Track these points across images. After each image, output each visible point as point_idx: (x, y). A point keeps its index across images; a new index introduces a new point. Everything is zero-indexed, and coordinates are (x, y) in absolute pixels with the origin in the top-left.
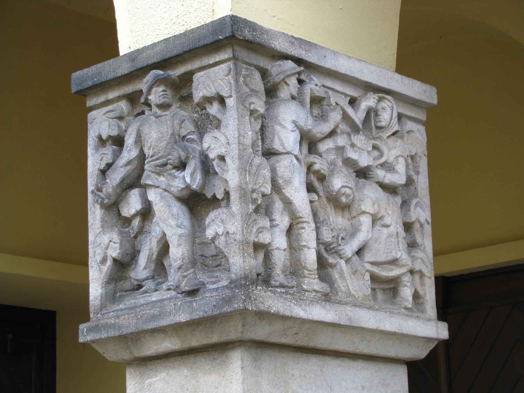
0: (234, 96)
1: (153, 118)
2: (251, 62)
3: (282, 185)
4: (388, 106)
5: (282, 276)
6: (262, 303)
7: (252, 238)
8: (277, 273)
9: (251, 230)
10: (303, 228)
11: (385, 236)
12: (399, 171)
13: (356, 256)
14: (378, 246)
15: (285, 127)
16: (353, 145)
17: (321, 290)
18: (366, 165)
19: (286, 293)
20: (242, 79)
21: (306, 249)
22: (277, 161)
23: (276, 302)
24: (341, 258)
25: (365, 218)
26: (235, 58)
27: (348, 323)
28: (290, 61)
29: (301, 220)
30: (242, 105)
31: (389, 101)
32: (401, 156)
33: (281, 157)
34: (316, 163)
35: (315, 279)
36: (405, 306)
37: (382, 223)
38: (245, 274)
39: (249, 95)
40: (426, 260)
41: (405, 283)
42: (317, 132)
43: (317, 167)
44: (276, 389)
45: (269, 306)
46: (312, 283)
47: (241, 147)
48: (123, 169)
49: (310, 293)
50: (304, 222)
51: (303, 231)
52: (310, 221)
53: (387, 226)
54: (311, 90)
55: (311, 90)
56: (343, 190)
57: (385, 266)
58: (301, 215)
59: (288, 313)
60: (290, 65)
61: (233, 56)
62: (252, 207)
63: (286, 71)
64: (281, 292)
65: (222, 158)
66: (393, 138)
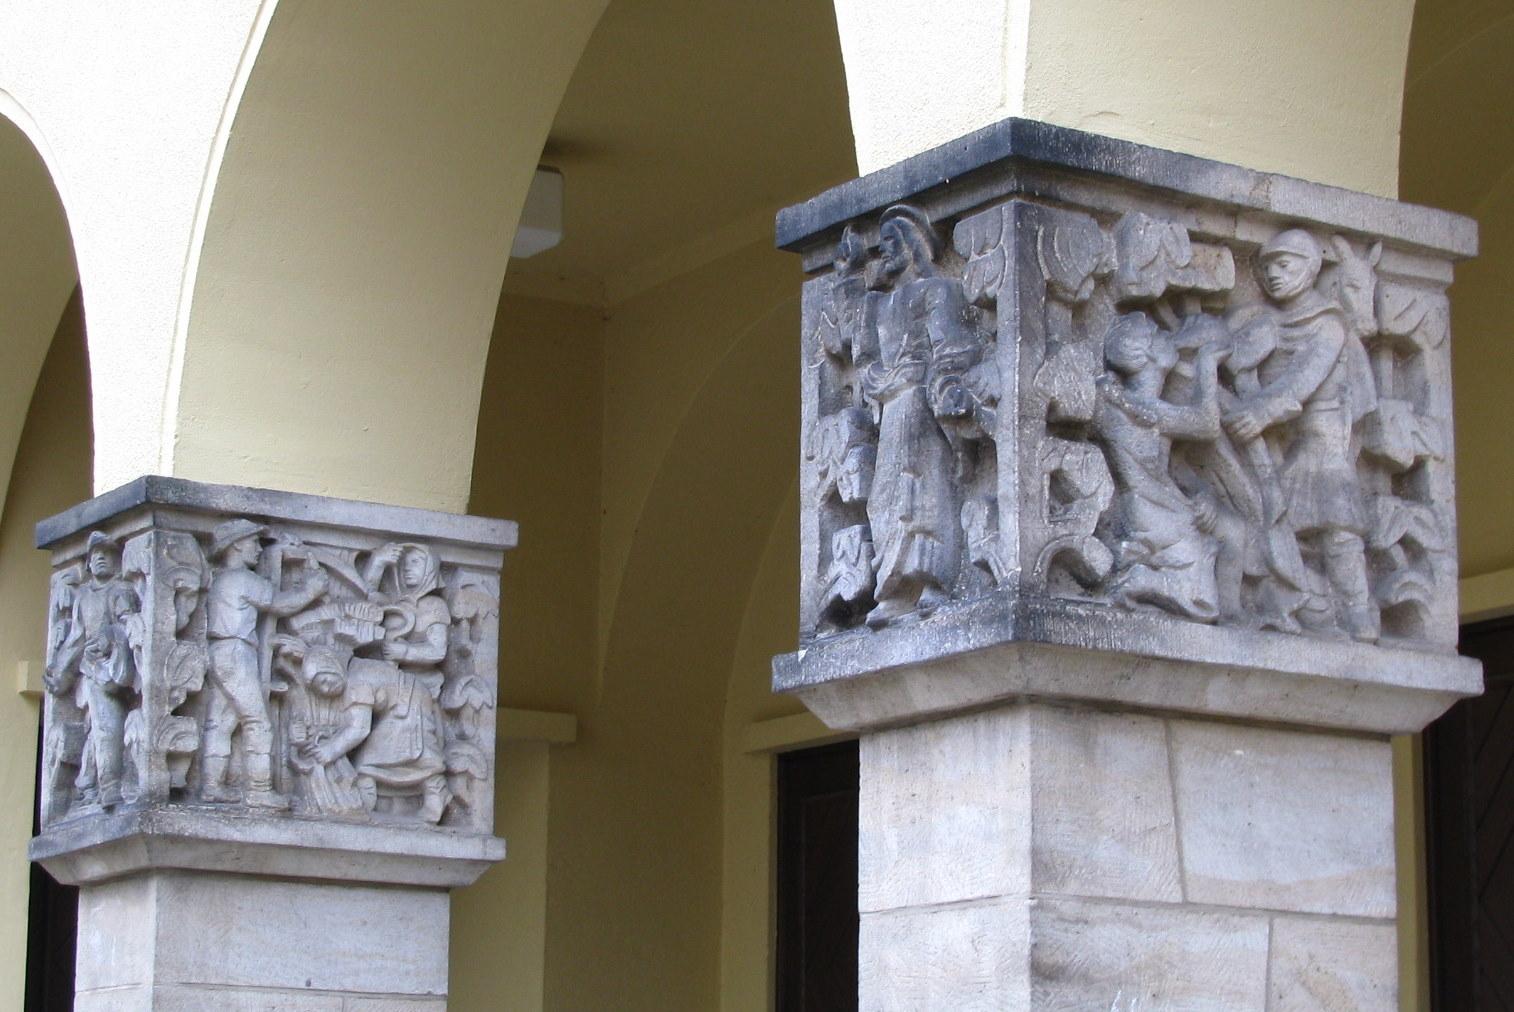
0: (152, 573)
1: (90, 591)
2: (184, 528)
3: (221, 677)
5: (218, 789)
6: (171, 825)
7: (165, 747)
9: (164, 737)
10: (252, 729)
11: (398, 730)
13: (346, 760)
15: (230, 606)
16: (348, 617)
17: (274, 805)
18: (370, 639)
19: (216, 811)
20: (165, 552)
21: (253, 756)
22: (218, 648)
23: (194, 823)
24: (319, 763)
26: (155, 524)
27: (315, 844)
28: (244, 521)
29: (249, 719)
31: (423, 552)
33: (223, 642)
37: (396, 713)
38: (150, 791)
39: (177, 570)
40: (478, 757)
43: (286, 649)
44: (210, 925)
47: (158, 636)
48: (69, 651)
50: (253, 722)
51: (252, 732)
52: (262, 720)
53: (403, 718)
54: (283, 551)
55: (283, 551)
56: (322, 678)
58: (247, 713)
59: (211, 835)
60: (244, 525)
61: (154, 523)
62: (168, 709)
63: (234, 534)
65: (139, 648)
66: (429, 599)
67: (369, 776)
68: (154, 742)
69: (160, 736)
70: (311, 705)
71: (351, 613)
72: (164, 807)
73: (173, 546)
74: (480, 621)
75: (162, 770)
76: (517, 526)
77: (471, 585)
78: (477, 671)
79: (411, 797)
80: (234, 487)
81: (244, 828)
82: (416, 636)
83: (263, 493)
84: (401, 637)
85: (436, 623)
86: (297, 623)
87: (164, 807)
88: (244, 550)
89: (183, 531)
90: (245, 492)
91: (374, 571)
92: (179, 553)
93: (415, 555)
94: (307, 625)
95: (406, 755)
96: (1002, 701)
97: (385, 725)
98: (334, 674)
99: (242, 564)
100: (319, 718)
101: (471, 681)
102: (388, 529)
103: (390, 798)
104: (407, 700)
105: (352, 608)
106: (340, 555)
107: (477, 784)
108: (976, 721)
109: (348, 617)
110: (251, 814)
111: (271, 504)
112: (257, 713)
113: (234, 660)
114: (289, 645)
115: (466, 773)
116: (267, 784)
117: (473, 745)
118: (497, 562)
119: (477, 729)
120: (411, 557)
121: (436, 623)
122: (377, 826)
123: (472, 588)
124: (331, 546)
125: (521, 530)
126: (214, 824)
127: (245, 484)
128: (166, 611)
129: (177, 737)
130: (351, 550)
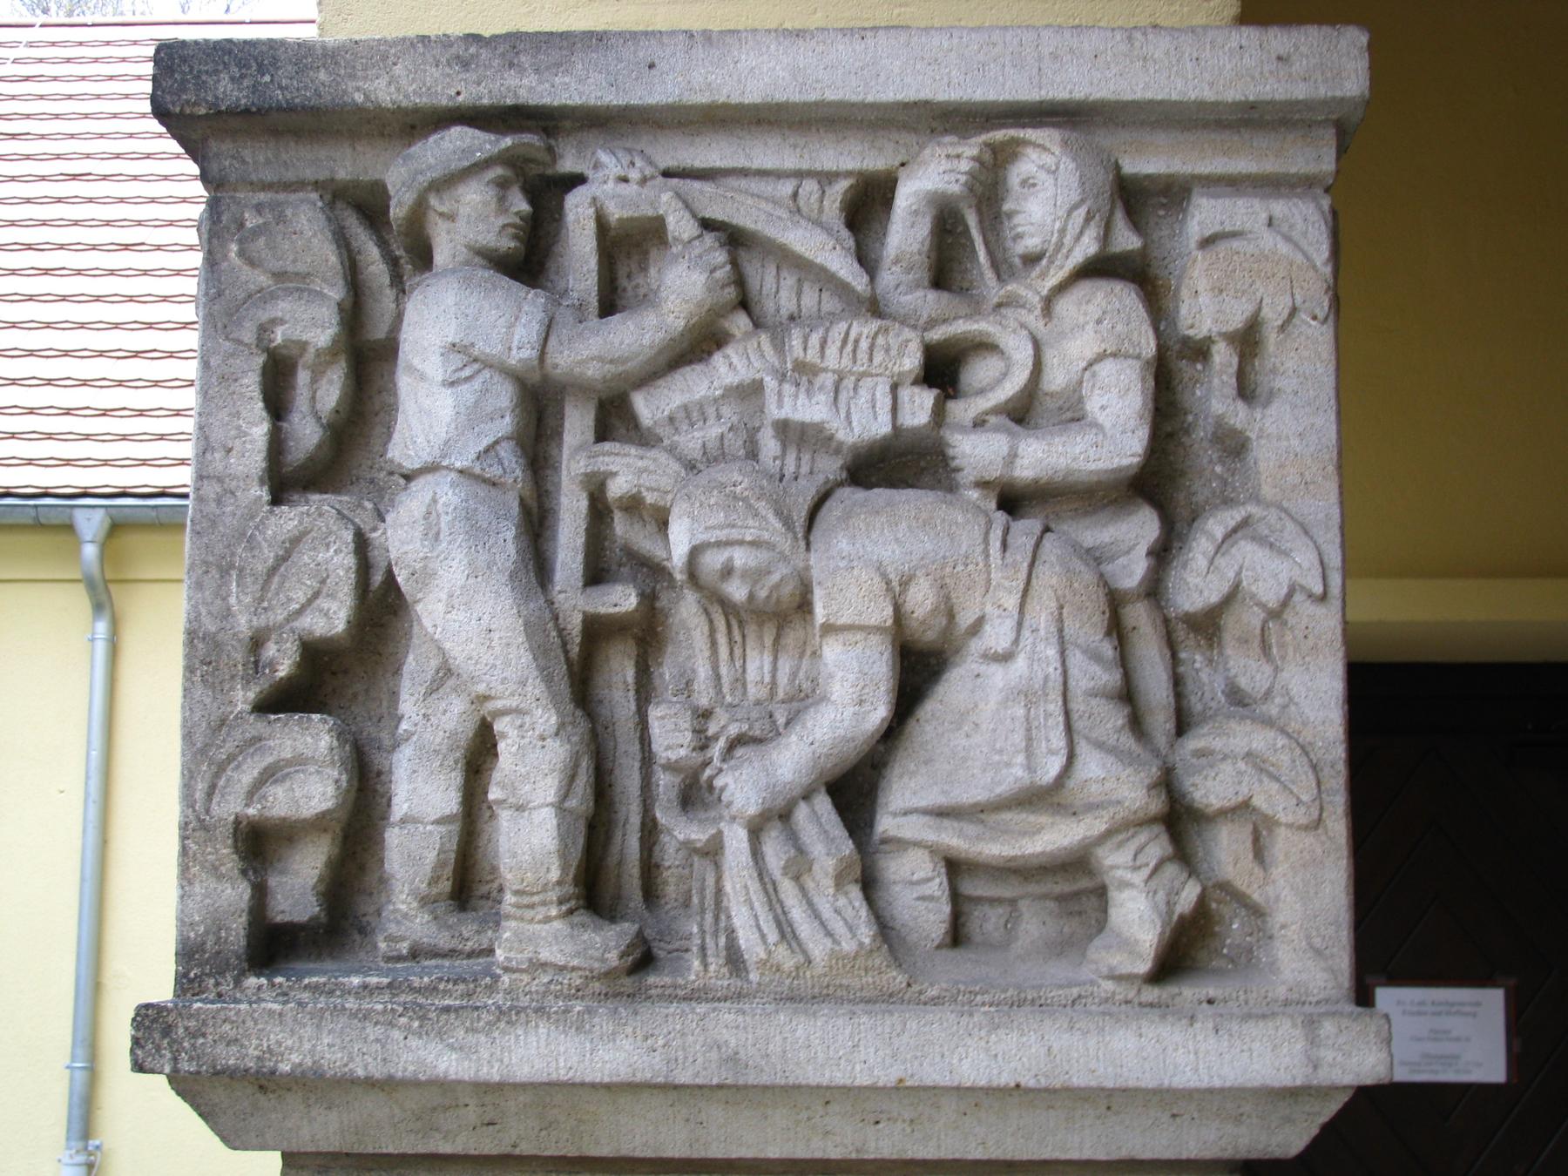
2: (290, 176)
4: (1042, 167)
8: (396, 911)
12: (1102, 418)
13: (823, 803)
14: (964, 742)
15: (423, 377)
17: (575, 962)
18: (881, 427)
25: (838, 648)
28: (456, 131)
30: (227, 338)
32: (1114, 355)
34: (614, 474)
35: (547, 920)
36: (1111, 969)
39: (264, 297)
41: (1119, 873)
42: (580, 363)
45: (270, 1050)
46: (537, 933)
49: (526, 978)
57: (1007, 816)
60: (460, 142)
62: (243, 697)
64: (365, 986)
66: (1084, 288)
67: (917, 844)
68: (199, 795)
69: (217, 775)
70: (714, 644)
71: (812, 356)
72: (227, 986)
73: (257, 232)
74: (1271, 338)
75: (220, 877)
76: (1363, 39)
77: (1234, 235)
78: (1267, 491)
79: (1076, 895)
80: (424, 39)
81: (471, 1039)
82: (1050, 404)
83: (513, 46)
84: (996, 410)
85: (1101, 357)
86: (648, 407)
87: (227, 986)
88: (464, 211)
89: (288, 187)
90: (458, 49)
91: (906, 232)
92: (272, 247)
93: (1028, 165)
94: (685, 408)
95: (1014, 776)
96: (650, 790)
97: (953, 691)
98: (755, 544)
99: (463, 254)
100: (740, 681)
101: (1245, 523)
102: (925, 94)
103: (1013, 902)
104: (1011, 602)
105: (815, 339)
106: (795, 195)
107: (1283, 844)
108: (601, 702)
109: (805, 372)
110: (508, 992)
111: (537, 71)
112: (512, 687)
113: (433, 535)
114: (627, 470)
115: (1244, 808)
116: (553, 895)
117: (1268, 722)
118: (1319, 158)
119: (1277, 670)
120: (1020, 170)
121: (1101, 357)
122: (936, 1001)
123: (1236, 244)
124: (762, 173)
125: (1377, 54)
126: (373, 1032)
127: (456, 29)
128: (238, 415)
129: (270, 775)
130: (826, 178)
